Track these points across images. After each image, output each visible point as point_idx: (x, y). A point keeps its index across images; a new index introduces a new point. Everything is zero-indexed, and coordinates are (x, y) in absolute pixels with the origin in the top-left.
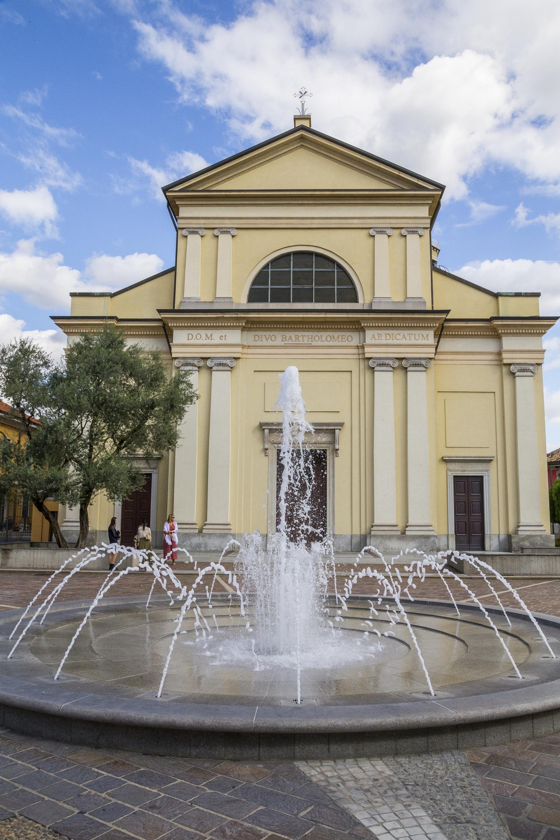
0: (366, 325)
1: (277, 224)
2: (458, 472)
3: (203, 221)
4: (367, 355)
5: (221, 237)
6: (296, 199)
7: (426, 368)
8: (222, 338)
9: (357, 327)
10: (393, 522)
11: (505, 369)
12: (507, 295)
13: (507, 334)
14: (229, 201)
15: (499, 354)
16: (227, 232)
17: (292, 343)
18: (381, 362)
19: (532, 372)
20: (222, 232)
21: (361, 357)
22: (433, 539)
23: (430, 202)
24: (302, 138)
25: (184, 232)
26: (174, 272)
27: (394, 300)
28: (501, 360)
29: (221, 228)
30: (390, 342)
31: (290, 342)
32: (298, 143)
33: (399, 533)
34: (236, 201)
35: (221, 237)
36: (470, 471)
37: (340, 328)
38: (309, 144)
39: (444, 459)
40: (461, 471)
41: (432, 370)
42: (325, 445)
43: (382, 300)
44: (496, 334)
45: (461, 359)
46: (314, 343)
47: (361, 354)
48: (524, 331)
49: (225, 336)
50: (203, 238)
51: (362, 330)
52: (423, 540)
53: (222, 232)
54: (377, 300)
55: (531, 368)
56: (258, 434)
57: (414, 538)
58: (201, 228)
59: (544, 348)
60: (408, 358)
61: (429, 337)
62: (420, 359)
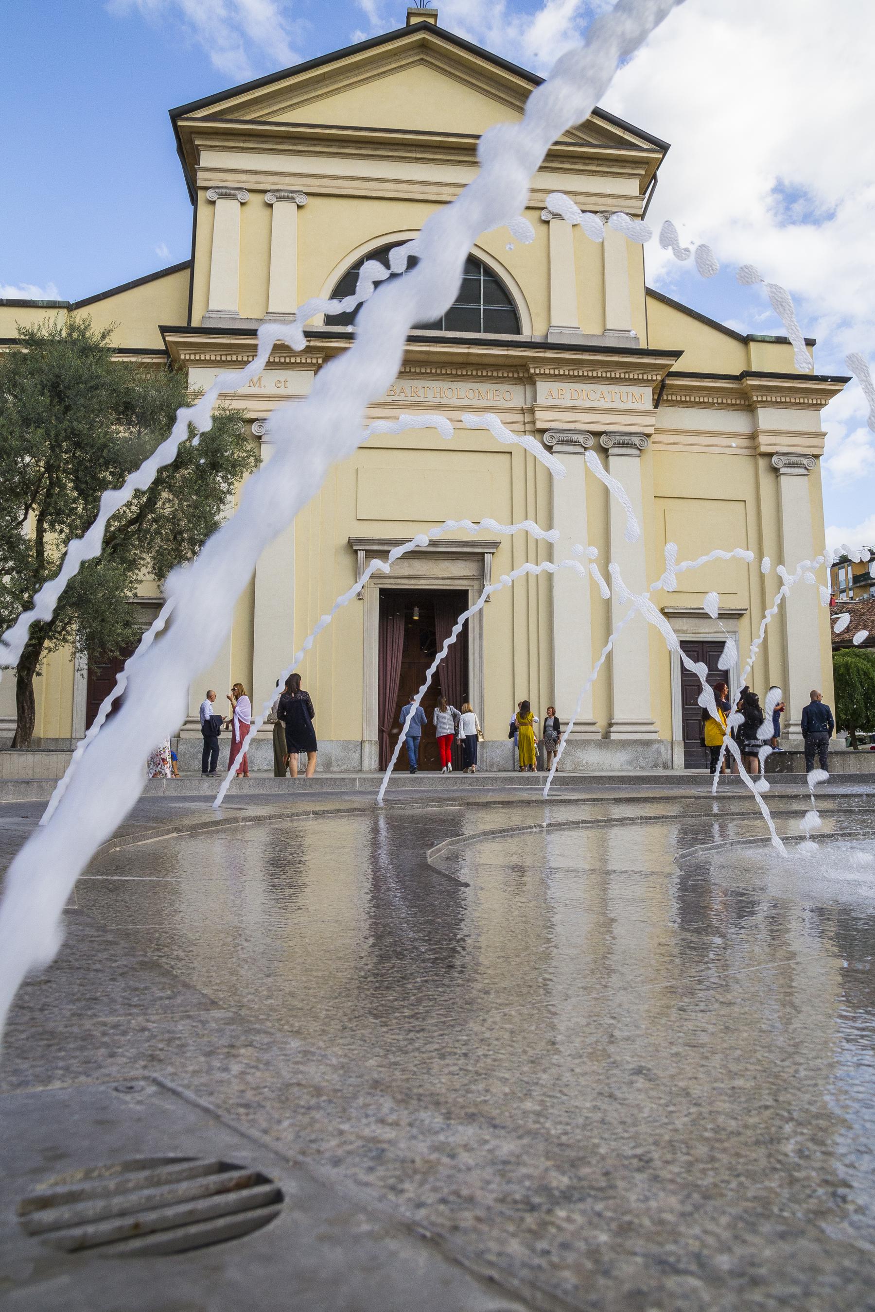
0: (537, 371)
1: (379, 190)
2: (688, 635)
3: (243, 177)
4: (540, 425)
5: (279, 206)
6: (414, 149)
7: (640, 450)
8: (279, 385)
9: (521, 375)
10: (588, 718)
11: (762, 463)
12: (764, 341)
13: (766, 404)
14: (291, 144)
15: (753, 436)
16: (288, 198)
17: (406, 399)
18: (564, 436)
19: (806, 468)
20: (280, 198)
21: (528, 427)
22: (656, 746)
23: (643, 172)
24: (423, 46)
25: (210, 195)
26: (188, 271)
27: (585, 332)
28: (755, 448)
29: (278, 191)
30: (579, 403)
31: (402, 397)
32: (413, 55)
33: (599, 737)
34: (304, 145)
35: (279, 206)
36: (706, 633)
37: (492, 377)
38: (435, 58)
39: (666, 611)
40: (693, 633)
41: (648, 456)
42: (465, 582)
43: (564, 331)
44: (747, 403)
45: (690, 442)
46: (445, 401)
47: (528, 423)
48: (793, 400)
49: (286, 381)
50: (245, 208)
51: (530, 381)
52: (640, 748)
53: (280, 198)
54: (557, 331)
55: (805, 461)
56: (346, 560)
57: (625, 744)
58: (240, 189)
59: (823, 430)
60: (611, 432)
61: (644, 396)
62: (631, 434)
